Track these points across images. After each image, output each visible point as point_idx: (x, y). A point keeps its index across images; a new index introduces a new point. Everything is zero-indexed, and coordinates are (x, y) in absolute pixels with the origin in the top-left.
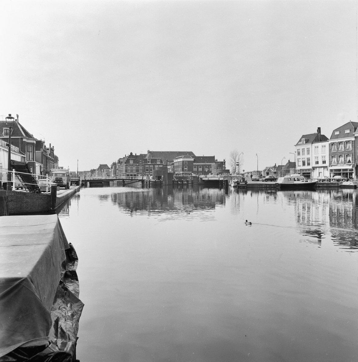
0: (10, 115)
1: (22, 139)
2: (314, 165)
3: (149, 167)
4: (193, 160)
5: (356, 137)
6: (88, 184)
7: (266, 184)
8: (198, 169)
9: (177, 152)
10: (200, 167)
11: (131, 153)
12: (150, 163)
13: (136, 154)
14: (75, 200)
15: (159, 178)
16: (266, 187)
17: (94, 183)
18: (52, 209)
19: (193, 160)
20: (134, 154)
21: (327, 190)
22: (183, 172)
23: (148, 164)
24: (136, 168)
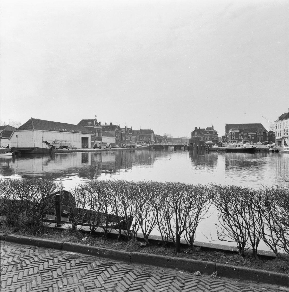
0: (42, 137)
1: (94, 127)
2: (283, 136)
3: (214, 136)
4: (239, 131)
6: (182, 148)
9: (248, 124)
10: (253, 136)
11: (196, 128)
12: (208, 134)
13: (200, 128)
15: (192, 144)
16: (222, 151)
19: (239, 131)
20: (198, 128)
21: (262, 152)
22: (232, 140)
23: (207, 134)
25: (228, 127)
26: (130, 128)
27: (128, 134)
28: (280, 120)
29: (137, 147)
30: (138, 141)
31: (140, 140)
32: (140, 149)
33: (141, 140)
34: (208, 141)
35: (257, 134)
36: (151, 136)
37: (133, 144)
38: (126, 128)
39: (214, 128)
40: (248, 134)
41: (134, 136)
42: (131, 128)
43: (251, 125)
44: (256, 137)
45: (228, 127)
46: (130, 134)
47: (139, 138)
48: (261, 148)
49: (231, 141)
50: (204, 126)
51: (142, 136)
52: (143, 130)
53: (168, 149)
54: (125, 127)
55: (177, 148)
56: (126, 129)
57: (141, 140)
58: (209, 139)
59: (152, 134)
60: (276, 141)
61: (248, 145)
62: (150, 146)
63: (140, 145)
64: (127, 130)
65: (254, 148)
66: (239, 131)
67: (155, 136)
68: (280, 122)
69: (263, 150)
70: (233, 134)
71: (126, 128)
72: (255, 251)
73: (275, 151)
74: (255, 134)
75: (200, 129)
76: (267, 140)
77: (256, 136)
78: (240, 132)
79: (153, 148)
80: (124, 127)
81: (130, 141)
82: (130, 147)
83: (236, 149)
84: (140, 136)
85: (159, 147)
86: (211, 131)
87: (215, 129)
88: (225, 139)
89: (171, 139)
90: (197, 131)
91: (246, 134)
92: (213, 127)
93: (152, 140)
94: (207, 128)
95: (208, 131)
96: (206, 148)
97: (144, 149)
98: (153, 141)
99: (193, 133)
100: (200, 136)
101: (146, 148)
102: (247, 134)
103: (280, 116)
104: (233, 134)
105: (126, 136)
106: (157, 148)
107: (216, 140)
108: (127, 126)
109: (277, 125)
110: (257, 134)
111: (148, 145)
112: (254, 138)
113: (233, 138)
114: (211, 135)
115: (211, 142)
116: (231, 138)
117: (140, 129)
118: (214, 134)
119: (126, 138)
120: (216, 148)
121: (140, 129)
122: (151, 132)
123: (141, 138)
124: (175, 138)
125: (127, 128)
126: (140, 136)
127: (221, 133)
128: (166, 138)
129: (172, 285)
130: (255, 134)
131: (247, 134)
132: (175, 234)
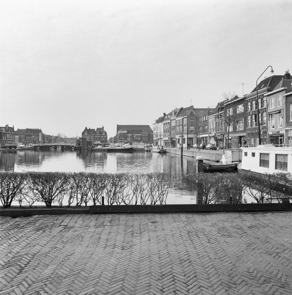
5: (171, 120)
7: (104, 149)
8: (137, 139)
10: (139, 137)
11: (86, 128)
13: (90, 128)
14: (270, 174)
17: (43, 147)
18: (285, 190)
20: (88, 128)
22: (120, 141)
24: (89, 138)
25: (119, 127)
26: (13, 127)
27: (9, 134)
28: (156, 123)
29: (20, 148)
30: (24, 141)
31: (26, 140)
32: (22, 149)
33: (27, 140)
34: (98, 141)
35: (142, 135)
36: (38, 136)
37: (14, 145)
38: (7, 127)
39: (104, 129)
40: (134, 135)
41: (16, 135)
42: (13, 127)
43: (140, 126)
44: (141, 139)
45: (119, 127)
46: (12, 134)
47: (26, 138)
48: (139, 148)
49: (120, 142)
50: (94, 127)
51: (29, 135)
52: (30, 129)
53: (57, 149)
54: (6, 126)
55: (66, 149)
56: (6, 128)
57: (27, 140)
58: (99, 139)
59: (40, 133)
60: (154, 141)
61: (127, 146)
62: (35, 147)
63: (23, 146)
64: (8, 129)
65: (133, 148)
66: (126, 132)
67: (44, 136)
68: (157, 125)
69: (140, 150)
70: (122, 135)
71: (7, 127)
72: (21, 206)
73: (148, 150)
74: (141, 135)
75: (90, 130)
76: (151, 140)
77: (142, 137)
78: (128, 133)
79: (40, 149)
80: (5, 126)
81: (12, 140)
82: (10, 147)
83: (117, 149)
84: (26, 136)
85: (46, 147)
86: (101, 132)
87: (105, 130)
88: (115, 140)
89: (62, 140)
90: (87, 132)
91: (132, 135)
92: (103, 127)
93: (40, 140)
94: (98, 129)
95: (98, 132)
96: (89, 148)
97: (28, 149)
98: (41, 141)
99: (83, 133)
100: (90, 136)
101: (30, 148)
102: (133, 135)
103: (157, 119)
104: (122, 135)
105: (6, 136)
106: (43, 148)
107: (105, 141)
108: (8, 125)
109: (155, 128)
110: (142, 135)
111: (34, 145)
112: (140, 138)
113: (121, 138)
114: (101, 136)
115: (100, 142)
116: (120, 138)
117: (27, 129)
118: (103, 134)
119: (7, 138)
120: (100, 148)
121: (27, 129)
122: (39, 131)
123: (27, 138)
124: (69, 138)
125: (8, 127)
126: (26, 136)
127: (111, 133)
128: (57, 138)
129: (66, 275)
130: (141, 135)
131: (133, 135)
132: (236, 282)
